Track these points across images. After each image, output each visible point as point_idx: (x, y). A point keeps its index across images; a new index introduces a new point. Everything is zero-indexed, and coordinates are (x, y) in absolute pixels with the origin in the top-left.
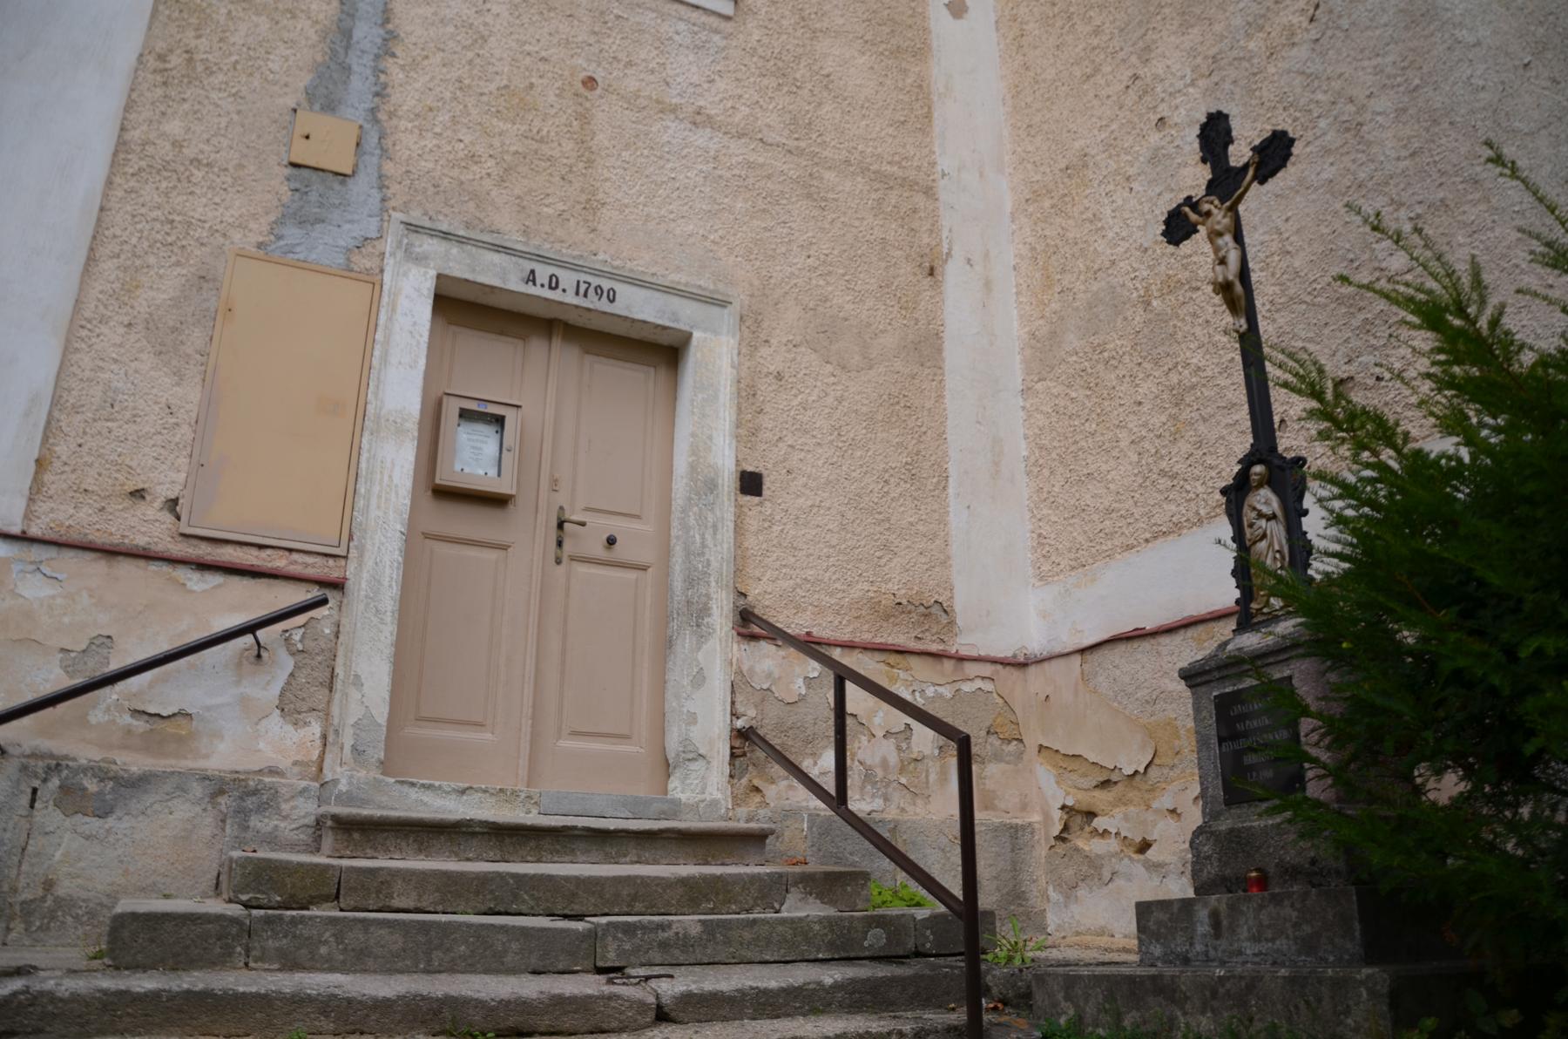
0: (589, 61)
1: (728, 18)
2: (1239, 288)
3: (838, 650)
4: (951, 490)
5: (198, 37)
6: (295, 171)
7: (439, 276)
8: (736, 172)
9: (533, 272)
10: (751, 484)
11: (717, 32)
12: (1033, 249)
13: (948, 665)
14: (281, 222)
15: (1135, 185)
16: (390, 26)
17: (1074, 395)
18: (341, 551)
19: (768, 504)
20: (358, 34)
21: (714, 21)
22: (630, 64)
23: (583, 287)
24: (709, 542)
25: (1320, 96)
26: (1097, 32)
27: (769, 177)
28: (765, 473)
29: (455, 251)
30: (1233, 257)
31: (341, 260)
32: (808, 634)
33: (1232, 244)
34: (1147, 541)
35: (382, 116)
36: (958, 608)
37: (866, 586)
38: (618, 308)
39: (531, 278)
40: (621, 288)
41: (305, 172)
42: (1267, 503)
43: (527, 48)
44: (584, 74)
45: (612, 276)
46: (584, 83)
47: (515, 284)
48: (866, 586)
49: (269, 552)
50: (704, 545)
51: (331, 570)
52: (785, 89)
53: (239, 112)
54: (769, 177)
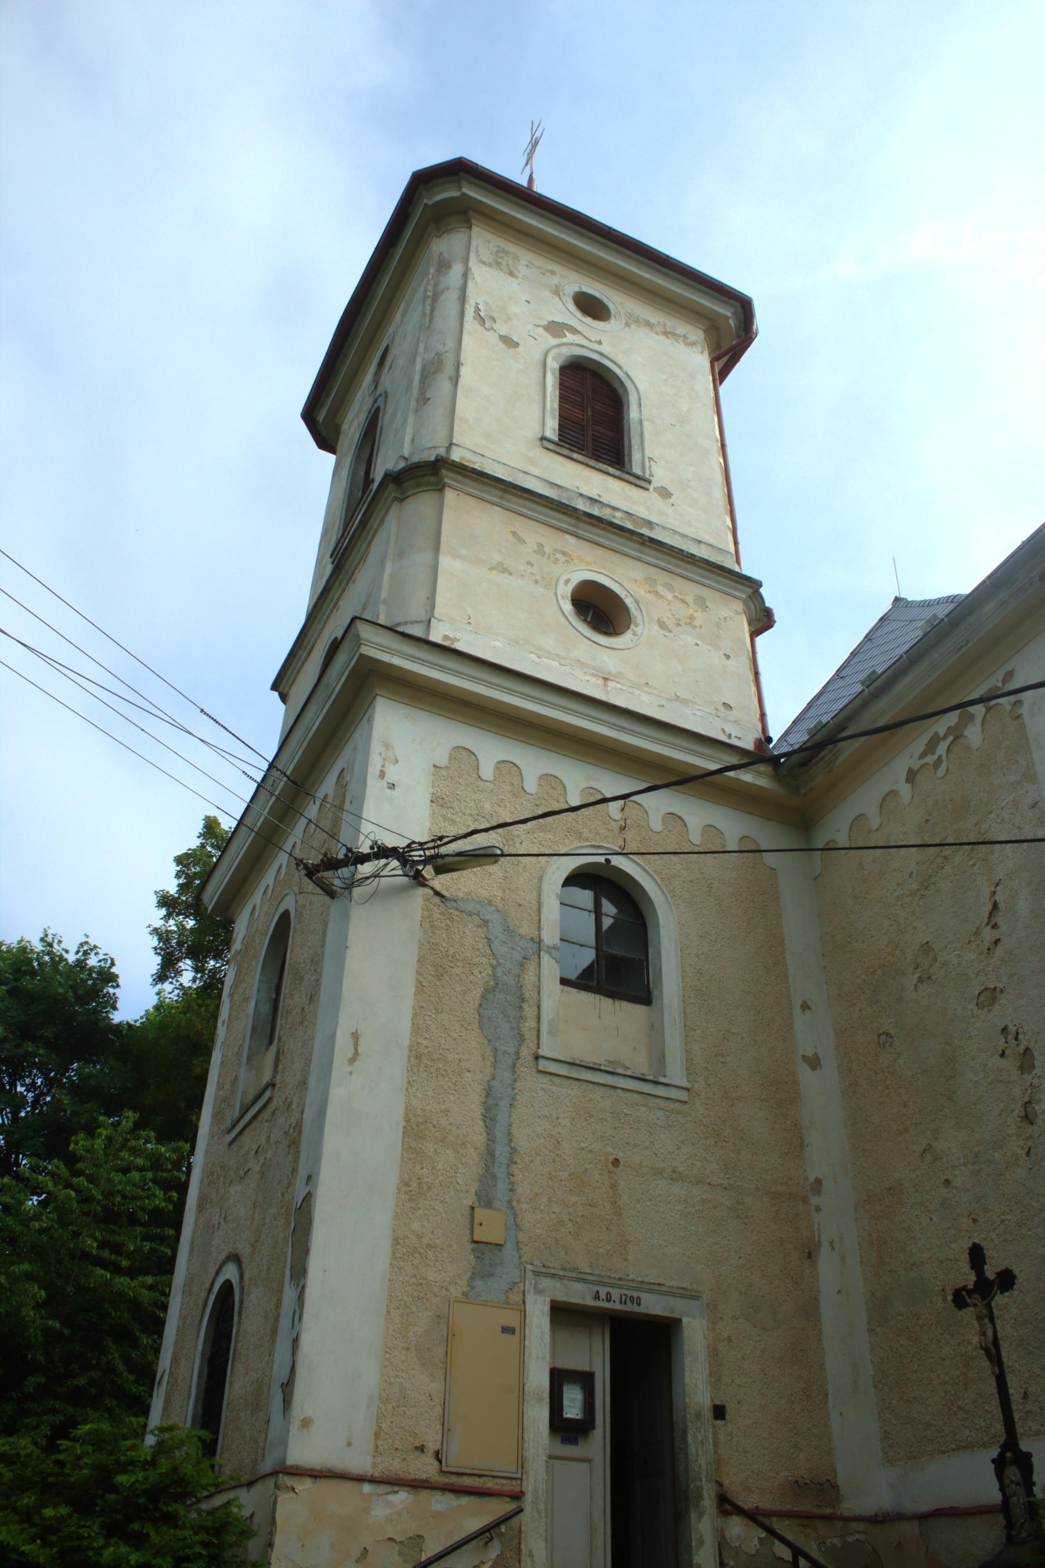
0: (614, 1148)
1: (685, 1102)
2: (993, 1350)
3: (774, 1519)
4: (830, 1404)
5: (422, 1168)
6: (476, 1246)
7: (552, 1301)
8: (698, 1208)
9: (598, 1292)
10: (719, 1412)
11: (679, 1113)
12: (870, 1235)
13: (839, 1524)
14: (472, 1278)
15: (934, 1217)
16: (512, 1144)
17: (902, 1342)
18: (519, 1476)
19: (729, 1425)
20: (497, 1153)
21: (677, 1106)
22: (636, 1145)
23: (624, 1297)
24: (700, 1453)
25: (1034, 1204)
26: (905, 1104)
27: (715, 1208)
28: (727, 1405)
29: (558, 1285)
30: (990, 1332)
31: (503, 1298)
32: (757, 1507)
33: (989, 1325)
34: (953, 1450)
35: (514, 1204)
36: (841, 1481)
37: (786, 1473)
38: (642, 1309)
39: (597, 1296)
40: (644, 1296)
41: (482, 1246)
42: (1014, 1475)
43: (583, 1145)
44: (612, 1158)
45: (638, 1289)
46: (613, 1163)
47: (590, 1302)
48: (786, 1473)
49: (484, 1478)
50: (697, 1455)
51: (514, 1487)
52: (719, 1145)
53: (446, 1212)
54: (715, 1208)
